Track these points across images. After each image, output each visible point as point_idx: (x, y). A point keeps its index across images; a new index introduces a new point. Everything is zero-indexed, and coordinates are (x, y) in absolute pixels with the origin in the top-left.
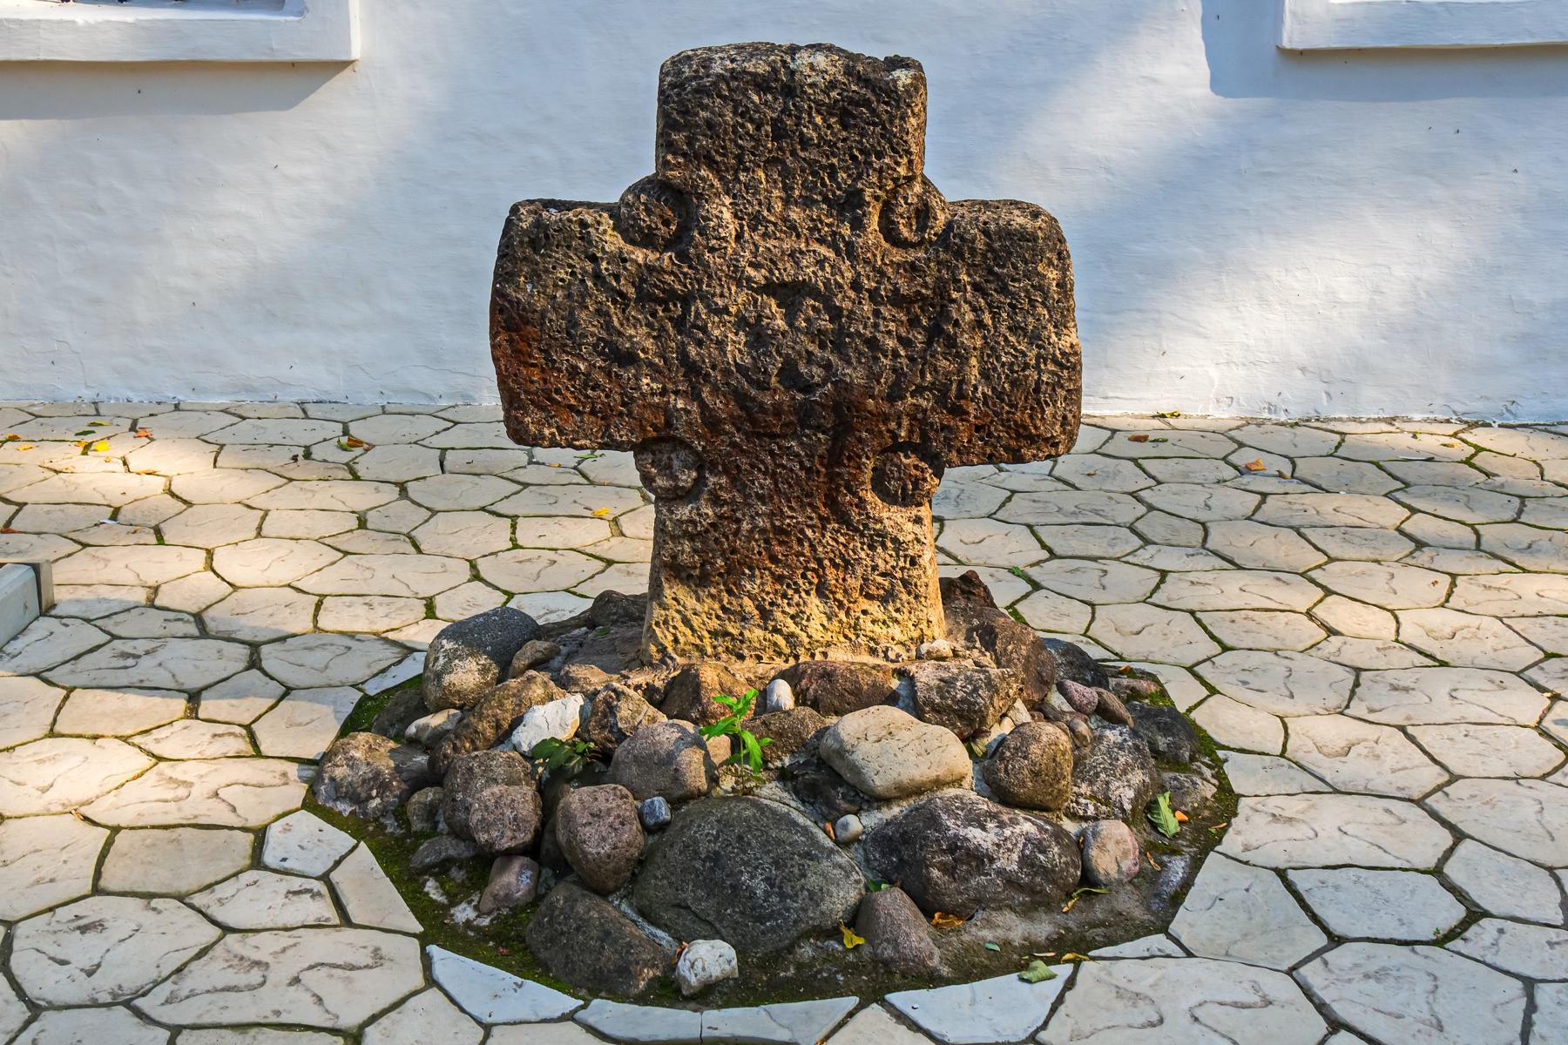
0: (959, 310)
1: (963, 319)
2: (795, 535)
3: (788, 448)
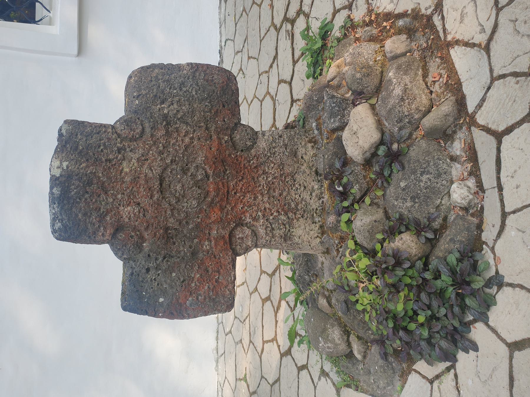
2: (271, 185)
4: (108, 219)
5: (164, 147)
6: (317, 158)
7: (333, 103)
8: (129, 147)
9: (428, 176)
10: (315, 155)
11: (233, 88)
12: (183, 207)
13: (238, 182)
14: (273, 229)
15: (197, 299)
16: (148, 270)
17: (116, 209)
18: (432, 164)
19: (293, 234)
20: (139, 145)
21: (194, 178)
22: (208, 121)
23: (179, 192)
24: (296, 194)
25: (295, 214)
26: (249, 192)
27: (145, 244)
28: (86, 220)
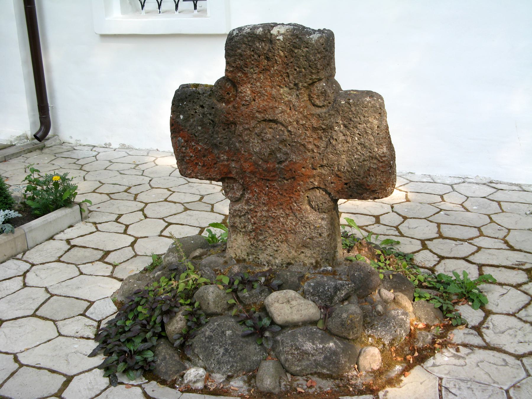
0: (337, 135)
4: (239, 74)
5: (303, 125)
6: (302, 266)
7: (328, 288)
8: (299, 94)
9: (221, 353)
10: (304, 265)
11: (365, 195)
12: (254, 139)
13: (277, 190)
14: (240, 217)
15: (183, 146)
16: (202, 107)
17: (248, 80)
18: (231, 359)
19: (239, 235)
20: (302, 102)
21: (277, 151)
22: (330, 168)
23: (264, 136)
24: (270, 242)
25: (254, 238)
26: (269, 199)
27: (224, 105)
28: (237, 56)
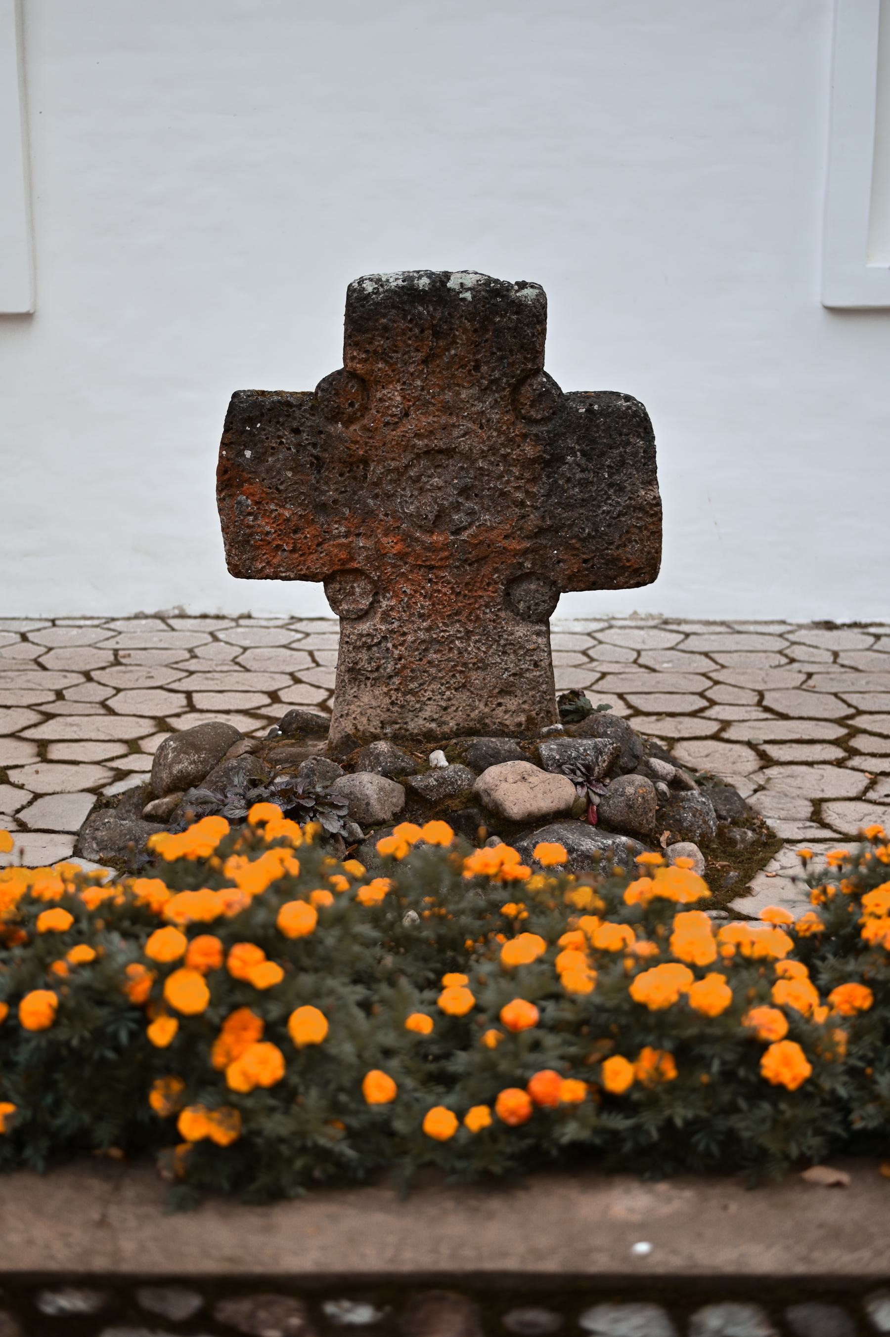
1: (575, 477)
3: (443, 577)
